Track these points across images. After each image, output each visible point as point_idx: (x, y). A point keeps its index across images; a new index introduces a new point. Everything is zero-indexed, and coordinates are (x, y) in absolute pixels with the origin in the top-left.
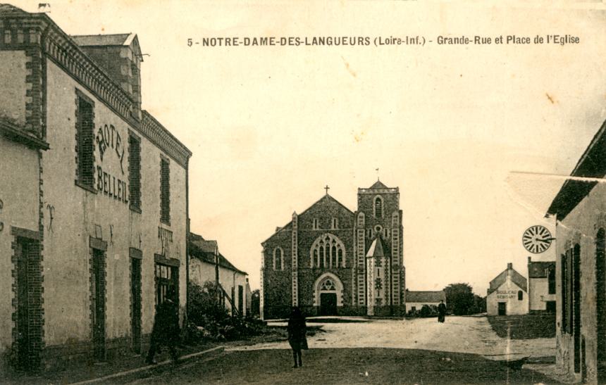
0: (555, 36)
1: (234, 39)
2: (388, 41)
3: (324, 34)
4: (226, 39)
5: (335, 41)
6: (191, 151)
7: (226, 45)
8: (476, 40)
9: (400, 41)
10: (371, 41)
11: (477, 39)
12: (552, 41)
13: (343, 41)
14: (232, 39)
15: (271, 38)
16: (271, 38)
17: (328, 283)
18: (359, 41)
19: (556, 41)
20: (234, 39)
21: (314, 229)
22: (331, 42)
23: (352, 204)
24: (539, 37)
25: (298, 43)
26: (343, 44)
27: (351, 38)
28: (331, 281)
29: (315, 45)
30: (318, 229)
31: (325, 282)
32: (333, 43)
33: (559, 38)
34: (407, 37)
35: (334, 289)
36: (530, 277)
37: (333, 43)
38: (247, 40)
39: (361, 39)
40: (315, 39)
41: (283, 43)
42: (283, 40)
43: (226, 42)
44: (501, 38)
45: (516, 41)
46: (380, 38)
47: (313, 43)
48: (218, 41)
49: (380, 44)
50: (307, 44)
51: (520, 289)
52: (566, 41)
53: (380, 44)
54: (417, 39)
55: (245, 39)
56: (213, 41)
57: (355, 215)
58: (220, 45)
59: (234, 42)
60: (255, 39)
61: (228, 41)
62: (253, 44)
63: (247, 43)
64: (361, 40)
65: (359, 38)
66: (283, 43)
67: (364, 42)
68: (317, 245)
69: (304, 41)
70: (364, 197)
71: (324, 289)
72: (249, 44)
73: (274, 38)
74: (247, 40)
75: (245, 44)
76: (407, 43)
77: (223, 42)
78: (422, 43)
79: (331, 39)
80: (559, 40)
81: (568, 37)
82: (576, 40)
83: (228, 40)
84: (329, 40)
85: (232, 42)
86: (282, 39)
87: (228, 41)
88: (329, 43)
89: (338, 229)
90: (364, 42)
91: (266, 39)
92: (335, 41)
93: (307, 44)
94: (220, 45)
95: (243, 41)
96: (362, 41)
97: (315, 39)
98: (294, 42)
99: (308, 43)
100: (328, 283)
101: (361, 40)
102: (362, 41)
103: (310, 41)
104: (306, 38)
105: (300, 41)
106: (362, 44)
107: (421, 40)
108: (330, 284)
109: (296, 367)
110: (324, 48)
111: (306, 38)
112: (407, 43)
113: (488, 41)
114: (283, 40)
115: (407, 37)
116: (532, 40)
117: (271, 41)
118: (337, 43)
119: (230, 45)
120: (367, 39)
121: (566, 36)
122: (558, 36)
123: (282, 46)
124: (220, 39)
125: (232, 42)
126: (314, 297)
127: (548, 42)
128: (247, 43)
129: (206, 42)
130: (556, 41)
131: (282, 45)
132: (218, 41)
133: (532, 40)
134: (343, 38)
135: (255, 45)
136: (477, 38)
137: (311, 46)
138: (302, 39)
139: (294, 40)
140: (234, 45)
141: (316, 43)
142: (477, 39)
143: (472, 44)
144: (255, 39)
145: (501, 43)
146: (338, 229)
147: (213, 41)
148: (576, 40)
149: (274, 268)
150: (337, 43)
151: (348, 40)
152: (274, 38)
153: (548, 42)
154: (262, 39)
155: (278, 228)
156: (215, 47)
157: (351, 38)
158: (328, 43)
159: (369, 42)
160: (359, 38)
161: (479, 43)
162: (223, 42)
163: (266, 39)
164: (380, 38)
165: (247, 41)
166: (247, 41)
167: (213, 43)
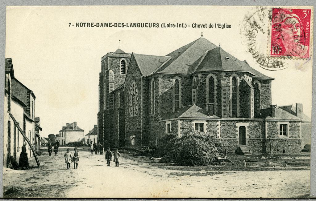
0: (219, 24)
1: (91, 23)
3: (136, 22)
4: (88, 23)
5: (142, 26)
6: (36, 97)
7: (88, 26)
9: (174, 26)
10: (160, 25)
12: (217, 27)
13: (145, 25)
18: (153, 25)
20: (91, 23)
22: (140, 26)
25: (123, 26)
27: (149, 24)
29: (131, 27)
33: (221, 25)
34: (178, 24)
39: (89, 24)
40: (131, 24)
42: (116, 24)
44: (206, 25)
46: (164, 24)
48: (84, 24)
49: (164, 27)
50: (127, 27)
52: (225, 27)
53: (164, 27)
54: (183, 25)
56: (81, 24)
58: (85, 26)
60: (102, 24)
61: (88, 25)
63: (98, 26)
65: (153, 24)
66: (116, 26)
67: (156, 26)
69: (126, 25)
73: (111, 23)
74: (98, 24)
75: (97, 26)
76: (178, 27)
77: (86, 25)
78: (185, 27)
79: (140, 24)
80: (221, 26)
81: (226, 24)
82: (229, 26)
83: (89, 24)
84: (139, 24)
85: (90, 25)
86: (97, 23)
87: (88, 25)
88: (139, 26)
90: (156, 26)
91: (107, 24)
92: (142, 26)
93: (127, 27)
94: (85, 26)
95: (114, 25)
97: (131, 24)
98: (121, 25)
102: (156, 25)
103: (129, 25)
105: (124, 25)
106: (155, 27)
107: (184, 25)
109: (116, 166)
110: (137, 28)
112: (178, 27)
114: (116, 24)
115: (178, 24)
117: (110, 25)
118: (142, 26)
121: (225, 24)
122: (221, 24)
124: (85, 23)
125: (90, 25)
127: (216, 27)
128: (98, 26)
129: (77, 25)
131: (97, 26)
132: (84, 24)
133: (207, 26)
137: (130, 27)
138: (125, 24)
139: (121, 24)
140: (91, 26)
141: (132, 26)
144: (102, 24)
145: (206, 27)
147: (81, 24)
148: (229, 26)
150: (142, 26)
151: (148, 25)
152: (111, 23)
153: (216, 27)
154: (105, 23)
155: (75, 123)
156: (144, 27)
157: (149, 24)
158: (138, 26)
159: (158, 26)
160: (153, 24)
162: (86, 25)
163: (107, 24)
164: (164, 24)
165: (98, 25)
166: (98, 25)
167: (81, 26)
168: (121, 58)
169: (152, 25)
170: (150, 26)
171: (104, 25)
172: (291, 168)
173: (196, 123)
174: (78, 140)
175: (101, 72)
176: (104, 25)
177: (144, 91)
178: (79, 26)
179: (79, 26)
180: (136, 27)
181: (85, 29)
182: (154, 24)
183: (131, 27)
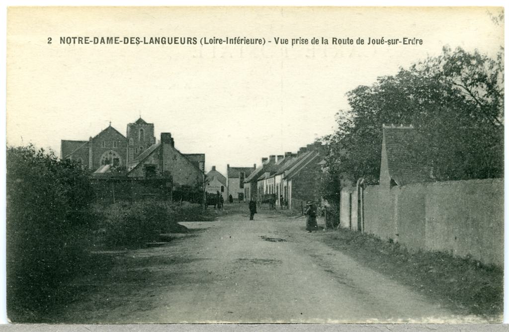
2: (211, 41)
4: (79, 38)
5: (168, 41)
7: (79, 43)
8: (333, 41)
10: (198, 41)
11: (334, 40)
14: (84, 39)
15: (116, 38)
16: (116, 38)
18: (188, 41)
19: (405, 42)
21: (102, 147)
22: (165, 41)
23: (123, 131)
24: (350, 39)
25: (138, 42)
26: (175, 43)
27: (181, 38)
30: (105, 147)
32: (167, 42)
36: (228, 177)
37: (167, 42)
38: (96, 39)
41: (126, 42)
43: (79, 40)
45: (324, 42)
47: (150, 42)
48: (72, 40)
49: (205, 43)
50: (145, 43)
51: (222, 185)
53: (205, 43)
55: (95, 38)
56: (69, 39)
57: (127, 140)
59: (85, 40)
60: (103, 38)
62: (101, 42)
64: (189, 40)
65: (188, 38)
66: (126, 42)
67: (192, 41)
68: (104, 157)
70: (132, 127)
72: (97, 43)
74: (96, 39)
75: (125, 43)
76: (227, 43)
77: (77, 40)
80: (407, 42)
84: (164, 39)
88: (164, 42)
89: (117, 148)
90: (192, 41)
91: (112, 38)
92: (168, 41)
93: (145, 43)
96: (192, 41)
97: (152, 38)
98: (135, 41)
99: (146, 42)
101: (189, 40)
102: (192, 41)
103: (148, 40)
104: (145, 38)
105: (140, 40)
106: (191, 43)
111: (145, 38)
112: (227, 43)
113: (395, 41)
115: (227, 38)
116: (310, 41)
117: (115, 40)
119: (336, 44)
120: (307, 40)
122: (407, 38)
123: (139, 45)
124: (74, 38)
129: (62, 40)
130: (405, 42)
131: (125, 43)
132: (72, 40)
134: (175, 38)
135: (152, 43)
136: (335, 40)
139: (135, 39)
141: (153, 42)
142: (334, 40)
143: (400, 45)
144: (103, 38)
146: (117, 148)
147: (69, 39)
148: (421, 42)
149: (92, 252)
150: (170, 42)
154: (108, 38)
157: (181, 38)
158: (67, 43)
159: (196, 41)
160: (188, 38)
161: (82, 43)
162: (77, 40)
163: (112, 38)
167: (69, 42)
170: (183, 42)
183: (103, 43)
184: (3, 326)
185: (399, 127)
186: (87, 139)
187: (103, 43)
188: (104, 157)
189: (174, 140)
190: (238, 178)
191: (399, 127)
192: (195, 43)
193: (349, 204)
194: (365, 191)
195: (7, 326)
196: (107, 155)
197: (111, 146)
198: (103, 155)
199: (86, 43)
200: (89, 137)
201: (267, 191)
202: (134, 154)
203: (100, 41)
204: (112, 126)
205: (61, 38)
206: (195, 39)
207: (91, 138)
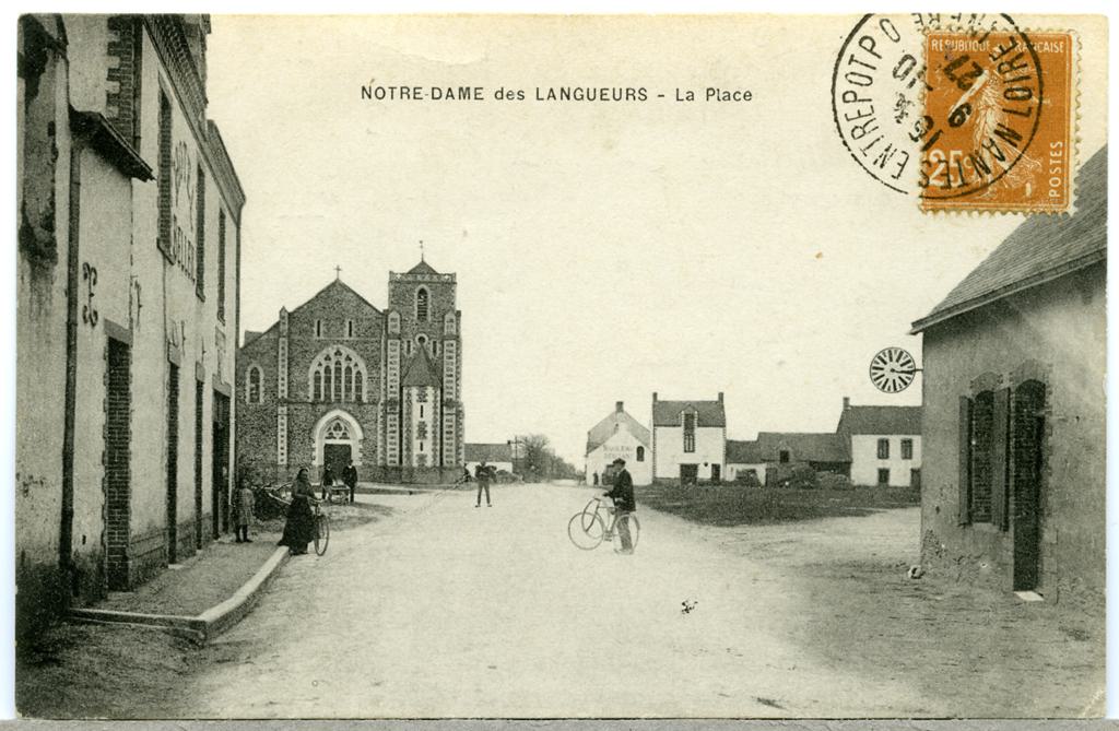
17: (338, 427)
28: (342, 425)
31: (334, 424)
35: (348, 438)
59: (415, 93)
65: (628, 90)
71: (331, 436)
90: (637, 95)
91: (468, 89)
100: (338, 427)
103: (544, 94)
108: (340, 430)
126: (313, 449)
132: (388, 92)
151: (610, 95)
154: (461, 89)
162: (397, 92)
168: (420, 283)
169: (624, 92)
170: (617, 97)
171: (456, 92)
172: (402, 488)
173: (349, 447)
174: (175, 218)
175: (208, 35)
176: (456, 92)
177: (361, 446)
178: (370, 97)
179: (370, 97)
180: (568, 97)
181: (853, 159)
182: (631, 92)
183: (450, 98)
184: (5, 724)
185: (741, 467)
186: (754, 438)
187: (450, 98)
188: (356, 365)
189: (462, 300)
190: (679, 426)
191: (741, 467)
192: (643, 97)
193: (231, 717)
194: (641, 531)
195: (12, 725)
196: (328, 358)
197: (339, 333)
198: (320, 358)
199: (415, 98)
200: (615, 403)
201: (422, 399)
202: (401, 356)
203: (444, 95)
204: (345, 280)
205: (364, 89)
206: (642, 92)
207: (283, 309)
